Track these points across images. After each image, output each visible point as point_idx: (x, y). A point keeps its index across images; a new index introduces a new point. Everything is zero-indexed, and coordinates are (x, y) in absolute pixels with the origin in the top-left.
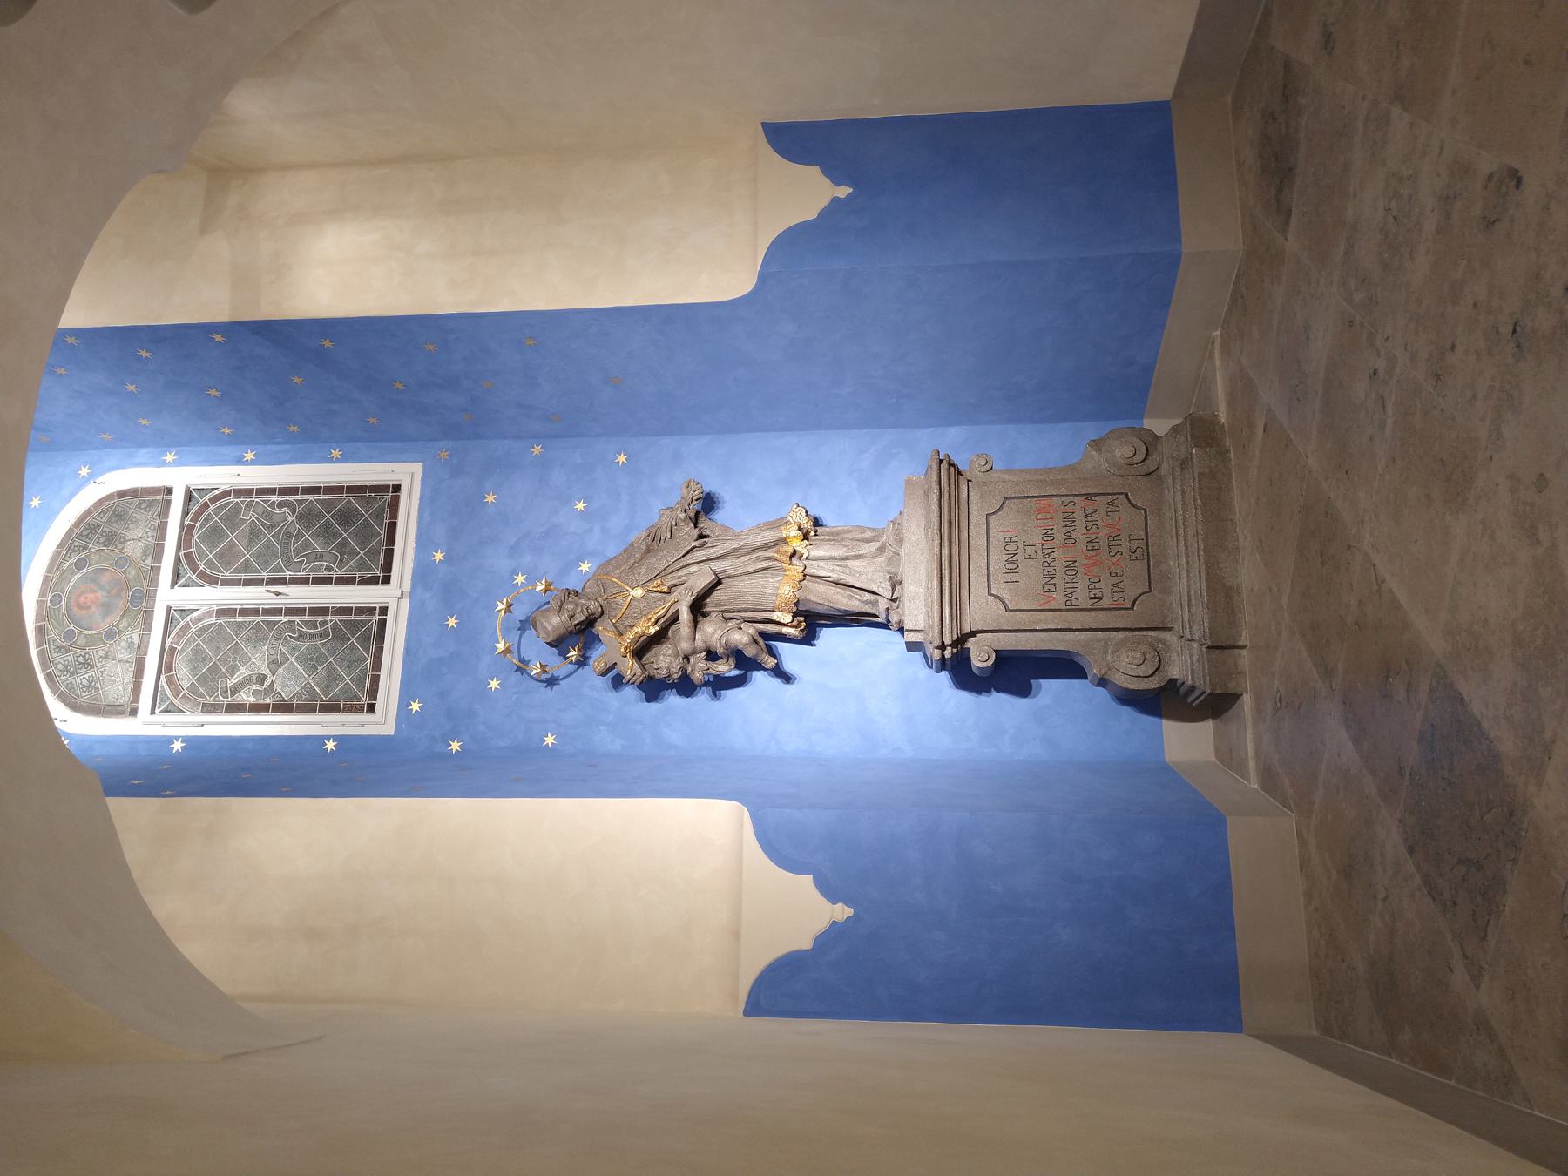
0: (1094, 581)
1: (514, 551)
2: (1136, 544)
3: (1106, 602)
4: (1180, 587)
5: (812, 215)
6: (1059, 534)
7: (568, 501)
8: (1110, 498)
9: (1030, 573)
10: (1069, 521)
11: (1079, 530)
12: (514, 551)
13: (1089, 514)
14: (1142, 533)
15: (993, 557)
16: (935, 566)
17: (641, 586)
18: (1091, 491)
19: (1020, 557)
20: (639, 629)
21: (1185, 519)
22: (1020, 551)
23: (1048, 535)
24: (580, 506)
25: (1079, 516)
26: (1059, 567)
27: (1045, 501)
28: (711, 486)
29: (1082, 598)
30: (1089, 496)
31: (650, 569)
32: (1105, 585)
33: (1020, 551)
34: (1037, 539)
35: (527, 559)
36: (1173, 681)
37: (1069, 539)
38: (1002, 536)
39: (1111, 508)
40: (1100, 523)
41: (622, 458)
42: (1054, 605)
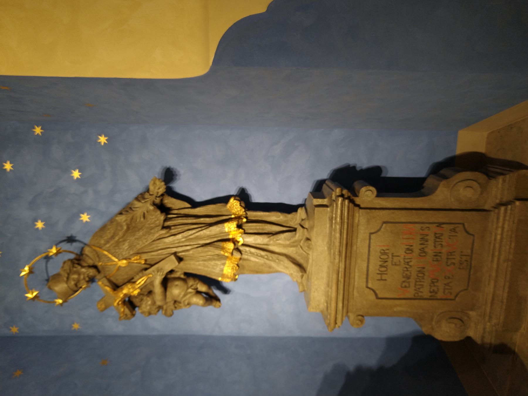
0: (433, 282)
1: (32, 205)
2: (464, 258)
3: (440, 295)
4: (489, 289)
5: (261, 8)
6: (416, 248)
7: (68, 171)
8: (452, 227)
9: (395, 275)
10: (424, 240)
11: (430, 248)
12: (32, 205)
13: (438, 237)
14: (469, 251)
15: (372, 262)
16: (335, 276)
17: (125, 259)
18: (441, 220)
19: (389, 264)
20: (125, 291)
21: (500, 246)
22: (390, 260)
23: (409, 250)
24: (76, 174)
25: (431, 238)
26: (414, 273)
27: (411, 226)
28: (172, 163)
29: (425, 293)
30: (440, 225)
31: (131, 247)
32: (440, 285)
33: (390, 260)
34: (401, 252)
35: (43, 211)
36: (469, 338)
37: (423, 252)
38: (378, 249)
39: (453, 234)
40: (444, 244)
41: (103, 139)
42: (408, 295)
